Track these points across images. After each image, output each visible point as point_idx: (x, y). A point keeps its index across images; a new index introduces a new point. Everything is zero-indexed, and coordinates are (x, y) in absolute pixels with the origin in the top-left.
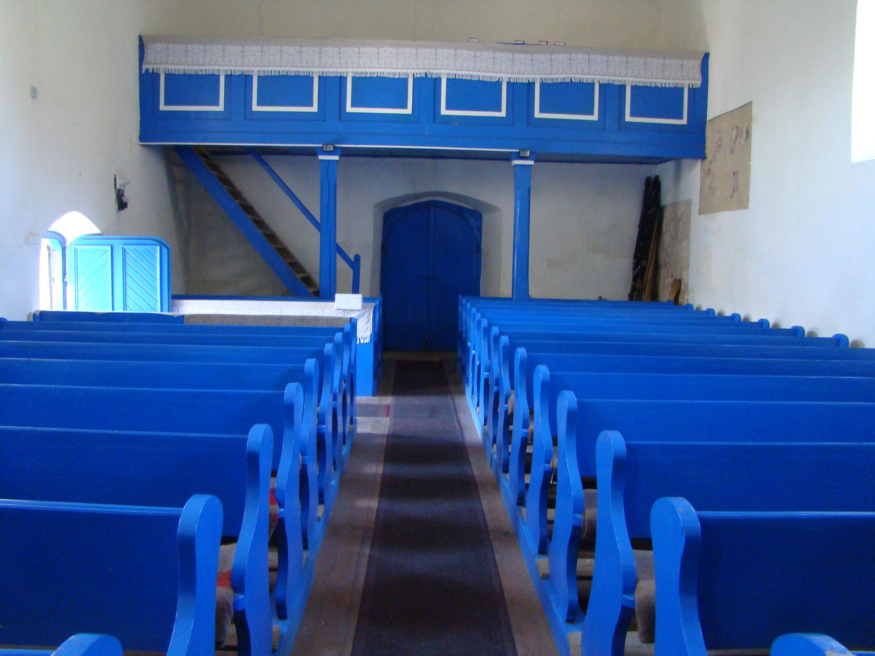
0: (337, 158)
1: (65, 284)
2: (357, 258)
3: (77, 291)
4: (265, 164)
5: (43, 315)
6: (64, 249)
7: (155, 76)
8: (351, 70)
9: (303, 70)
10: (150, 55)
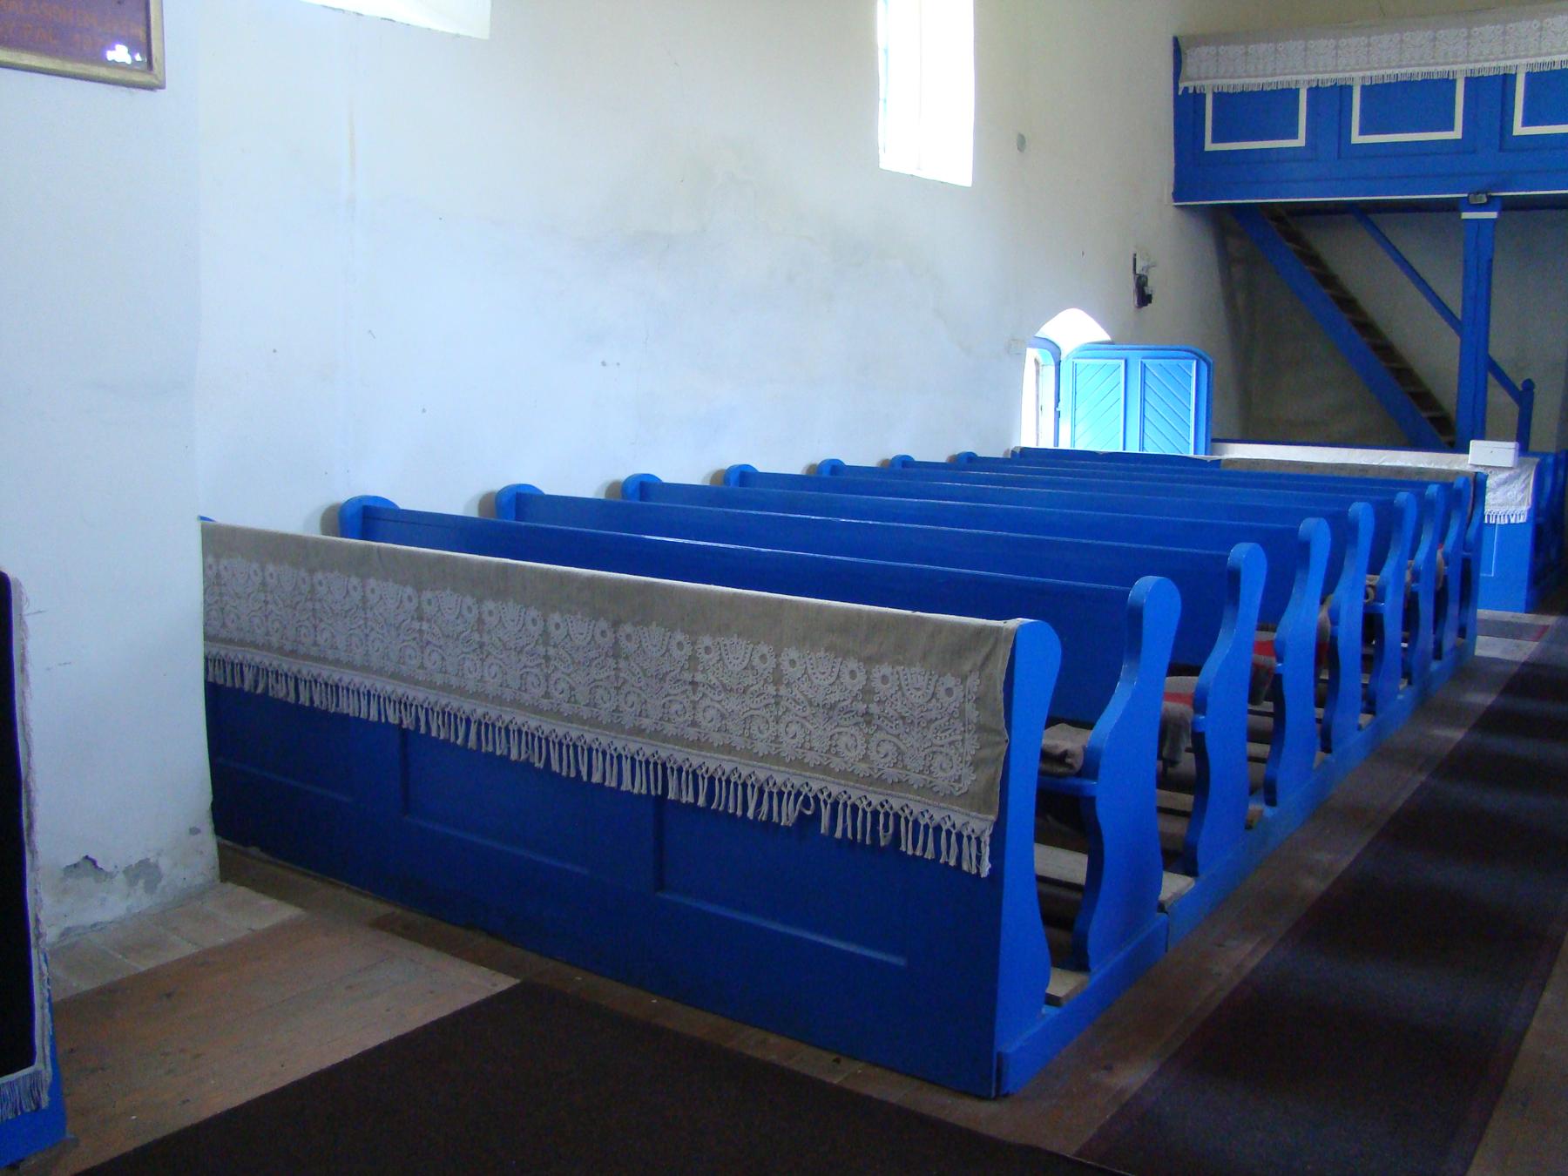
0: (1493, 215)
1: (1058, 415)
2: (1529, 386)
3: (1074, 426)
4: (1374, 229)
5: (1025, 452)
6: (1058, 364)
7: (1198, 98)
8: (1524, 61)
9: (1437, 70)
10: (1189, 68)
